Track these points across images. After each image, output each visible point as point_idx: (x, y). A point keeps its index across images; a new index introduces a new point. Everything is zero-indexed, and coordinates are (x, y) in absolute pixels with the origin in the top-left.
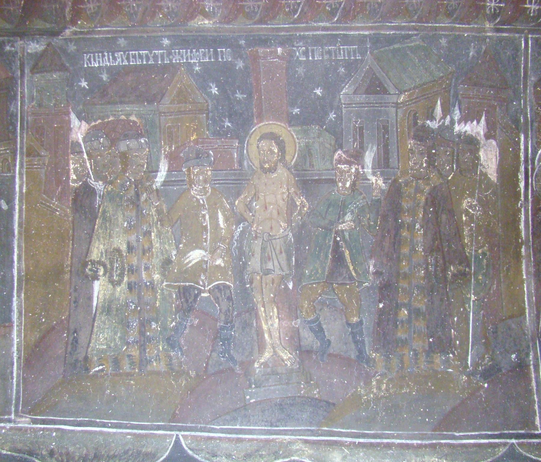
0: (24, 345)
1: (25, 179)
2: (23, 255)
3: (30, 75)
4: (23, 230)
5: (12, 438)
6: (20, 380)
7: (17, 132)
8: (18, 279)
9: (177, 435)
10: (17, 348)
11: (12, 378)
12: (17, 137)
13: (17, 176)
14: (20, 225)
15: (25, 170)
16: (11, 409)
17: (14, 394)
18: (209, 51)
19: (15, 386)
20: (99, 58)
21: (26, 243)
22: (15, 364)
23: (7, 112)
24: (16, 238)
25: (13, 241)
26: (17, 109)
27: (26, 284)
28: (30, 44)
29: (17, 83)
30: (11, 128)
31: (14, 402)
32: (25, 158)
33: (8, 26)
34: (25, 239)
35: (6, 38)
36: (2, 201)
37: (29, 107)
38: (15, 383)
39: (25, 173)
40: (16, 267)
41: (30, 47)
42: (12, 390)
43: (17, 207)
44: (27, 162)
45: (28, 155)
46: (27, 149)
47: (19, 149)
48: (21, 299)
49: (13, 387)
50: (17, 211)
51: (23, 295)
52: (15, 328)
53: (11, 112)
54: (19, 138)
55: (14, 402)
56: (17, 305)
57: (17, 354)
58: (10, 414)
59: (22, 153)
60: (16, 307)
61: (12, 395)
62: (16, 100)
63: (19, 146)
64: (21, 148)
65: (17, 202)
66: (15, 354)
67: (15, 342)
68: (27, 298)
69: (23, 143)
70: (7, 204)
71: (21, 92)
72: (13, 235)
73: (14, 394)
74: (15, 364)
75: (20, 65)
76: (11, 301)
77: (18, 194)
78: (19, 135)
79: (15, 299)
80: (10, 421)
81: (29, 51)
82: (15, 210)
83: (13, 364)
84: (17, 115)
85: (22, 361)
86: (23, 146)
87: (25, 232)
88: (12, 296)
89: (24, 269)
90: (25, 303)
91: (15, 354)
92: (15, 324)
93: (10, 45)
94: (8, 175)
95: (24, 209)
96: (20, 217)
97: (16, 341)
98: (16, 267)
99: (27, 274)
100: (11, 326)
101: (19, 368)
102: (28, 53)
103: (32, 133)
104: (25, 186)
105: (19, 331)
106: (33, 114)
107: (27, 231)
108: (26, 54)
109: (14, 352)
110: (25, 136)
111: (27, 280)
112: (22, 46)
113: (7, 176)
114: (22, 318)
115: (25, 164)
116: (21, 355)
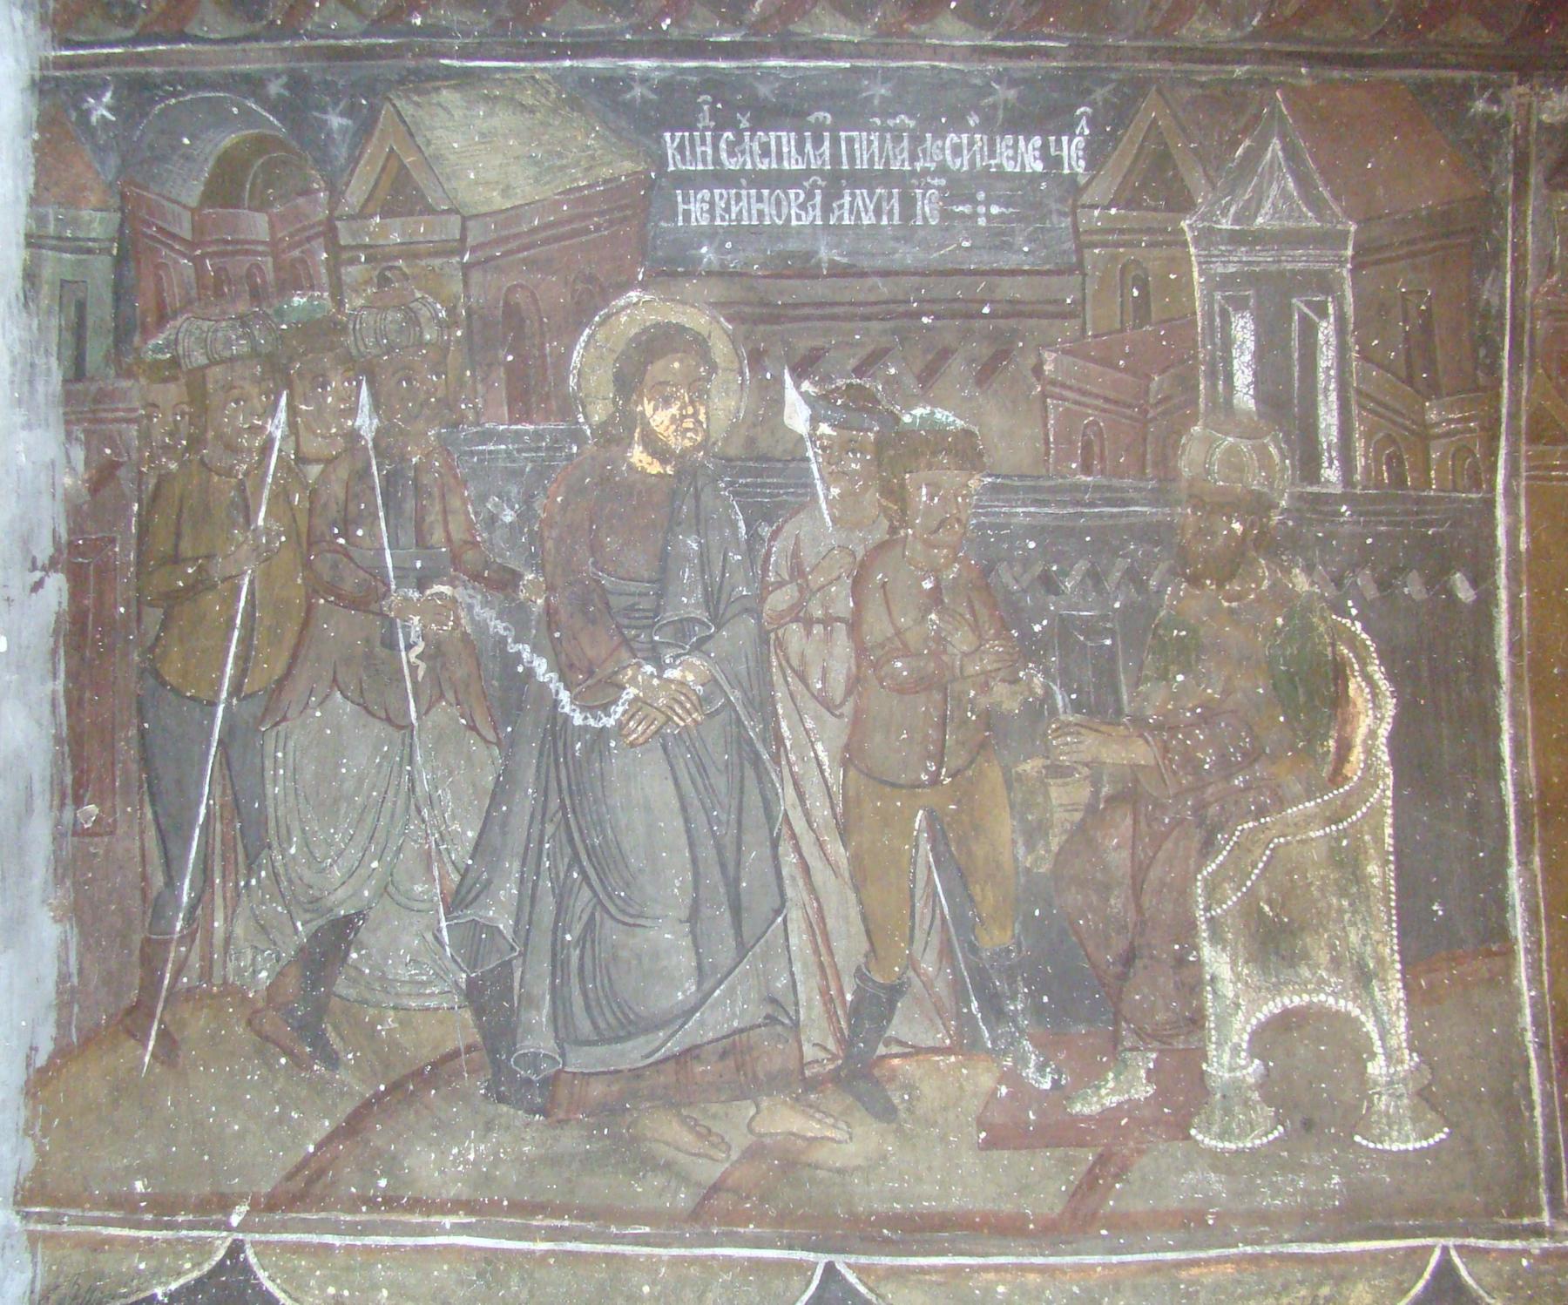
0: (1553, 1008)
1: (1523, 511)
2: (1530, 740)
3: (1545, 192)
4: (1525, 663)
5: (1556, 1283)
6: (1553, 1111)
7: (1501, 366)
8: (1516, 812)
9: (1445, 1250)
10: (1534, 1016)
11: (1531, 1108)
12: (1500, 381)
13: (1500, 500)
14: (1515, 650)
15: (1523, 483)
16: (1537, 1198)
17: (1541, 1151)
18: (971, 143)
19: (1540, 1129)
20: (703, 143)
21: (1536, 704)
22: (1534, 1063)
23: (1473, 303)
24: (1506, 687)
25: (1495, 697)
26: (1502, 296)
27: (1544, 826)
28: (1547, 97)
29: (1503, 216)
30: (1482, 352)
31: (1542, 1176)
32: (1523, 448)
33: (1484, 35)
34: (1533, 693)
35: (1474, 74)
36: (1458, 575)
37: (1536, 291)
38: (1539, 1120)
39: (1523, 492)
40: (1508, 777)
41: (1549, 104)
42: (1533, 1144)
43: (1503, 595)
44: (1528, 458)
45: (1533, 438)
46: (1530, 418)
47: (1504, 419)
48: (1532, 870)
49: (1535, 1132)
50: (1504, 606)
51: (1537, 859)
52: (1522, 958)
53: (1481, 304)
54: (1505, 383)
55: (1542, 1176)
56: (1523, 888)
57: (1536, 1034)
58: (1536, 1211)
59: (1513, 433)
60: (1517, 897)
61: (1535, 1158)
62: (1500, 269)
63: (1504, 411)
64: (1514, 416)
65: (1502, 580)
66: (1529, 1035)
67: (1526, 999)
68: (1548, 868)
69: (1519, 401)
70: (1474, 583)
71: (1515, 246)
72: (1496, 681)
73: (1541, 1151)
74: (1534, 1063)
75: (1516, 162)
76: (1502, 877)
77: (1503, 557)
78: (1506, 376)
79: (1513, 870)
80: (1538, 1232)
81: (1544, 117)
82: (1497, 606)
83: (1527, 1064)
84: (1501, 314)
85: (1552, 1055)
86: (1519, 410)
87: (1530, 669)
88: (1504, 862)
89: (1534, 781)
90: (1545, 882)
91: (1529, 1035)
92: (1520, 947)
93: (1486, 95)
94: (1473, 496)
95: (1525, 603)
96: (1514, 624)
97: (1527, 995)
98: (1508, 777)
99: (1542, 795)
100: (1508, 953)
101: (1545, 1076)
102: (1540, 123)
103: (1545, 370)
104: (1524, 531)
105: (1535, 966)
106: (1550, 312)
107: (1537, 667)
108: (1534, 126)
109: (1524, 1029)
110: (1525, 378)
111: (1546, 815)
112: (1523, 100)
113: (1470, 501)
114: (1539, 925)
115: (1523, 464)
116: (1546, 1036)
